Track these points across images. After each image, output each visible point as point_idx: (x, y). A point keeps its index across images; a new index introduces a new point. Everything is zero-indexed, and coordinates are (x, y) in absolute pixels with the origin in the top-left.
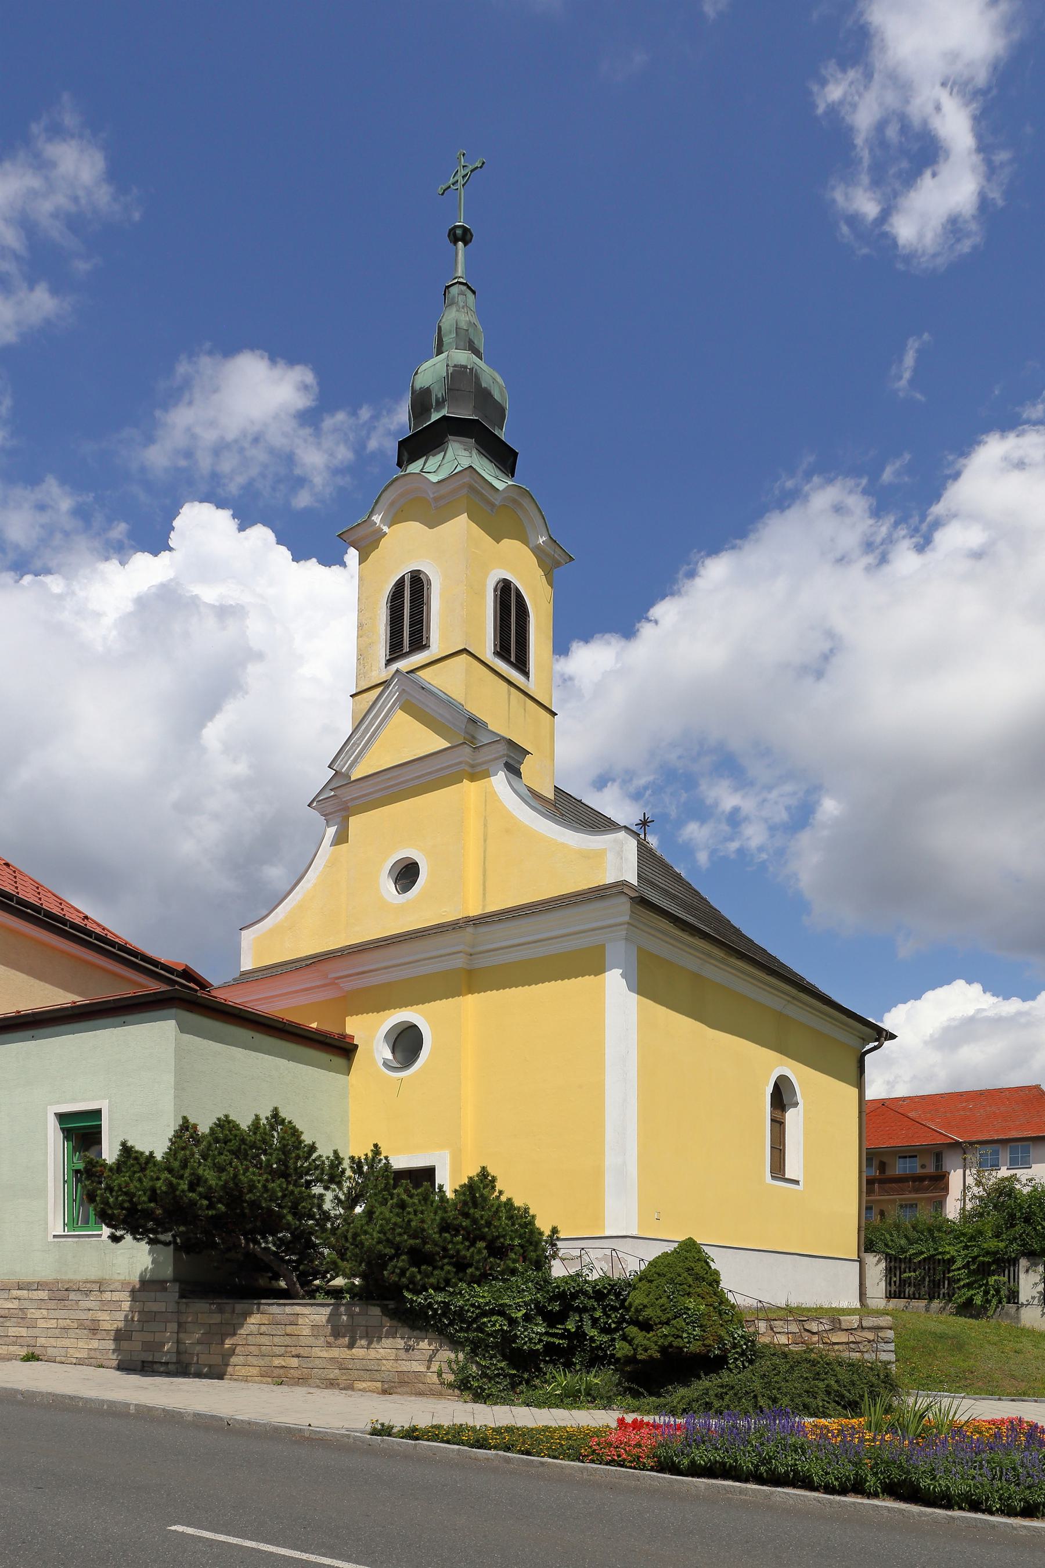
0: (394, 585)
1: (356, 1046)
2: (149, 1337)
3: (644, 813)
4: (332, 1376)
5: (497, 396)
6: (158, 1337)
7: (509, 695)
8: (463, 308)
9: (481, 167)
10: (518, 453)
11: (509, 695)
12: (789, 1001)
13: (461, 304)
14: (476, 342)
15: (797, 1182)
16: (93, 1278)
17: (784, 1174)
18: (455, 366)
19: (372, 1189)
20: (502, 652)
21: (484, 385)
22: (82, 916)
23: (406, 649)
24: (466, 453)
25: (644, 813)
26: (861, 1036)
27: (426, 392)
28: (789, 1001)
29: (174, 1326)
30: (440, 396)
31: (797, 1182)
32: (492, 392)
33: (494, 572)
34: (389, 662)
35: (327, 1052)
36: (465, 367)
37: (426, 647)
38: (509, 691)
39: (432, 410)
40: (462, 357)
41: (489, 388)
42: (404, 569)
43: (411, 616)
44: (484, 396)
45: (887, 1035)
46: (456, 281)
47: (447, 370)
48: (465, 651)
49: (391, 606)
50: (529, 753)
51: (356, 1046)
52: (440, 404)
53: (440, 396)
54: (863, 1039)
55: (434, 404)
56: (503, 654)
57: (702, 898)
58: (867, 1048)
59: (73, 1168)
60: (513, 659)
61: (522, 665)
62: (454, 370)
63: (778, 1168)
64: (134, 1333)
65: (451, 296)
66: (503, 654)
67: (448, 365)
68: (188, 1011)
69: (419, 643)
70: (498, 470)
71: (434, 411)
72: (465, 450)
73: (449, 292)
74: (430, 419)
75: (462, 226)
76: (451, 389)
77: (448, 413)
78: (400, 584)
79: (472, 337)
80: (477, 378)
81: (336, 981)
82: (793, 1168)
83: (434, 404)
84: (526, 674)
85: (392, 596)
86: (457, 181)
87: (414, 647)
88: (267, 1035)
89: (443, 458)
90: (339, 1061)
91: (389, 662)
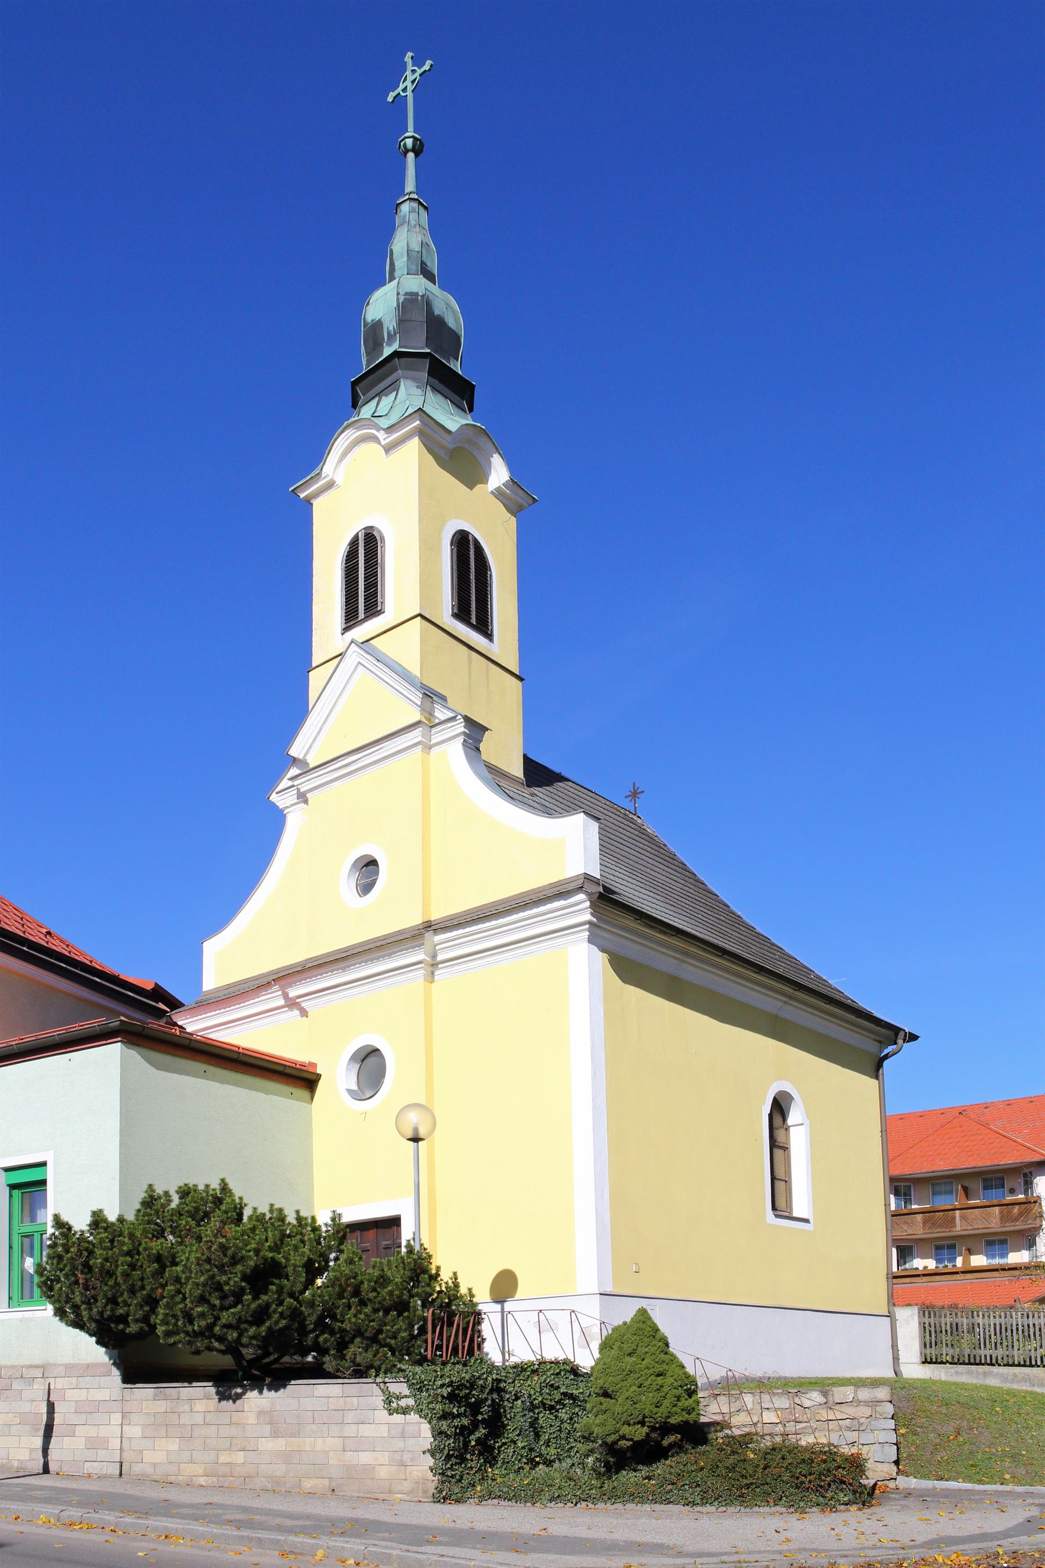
0: (349, 544)
1: (319, 1076)
2: (92, 1432)
3: (634, 783)
4: (279, 1474)
5: (451, 323)
6: (103, 1432)
7: (470, 662)
8: (415, 227)
9: (429, 70)
10: (474, 386)
11: (470, 662)
12: (785, 1002)
13: (413, 223)
14: (429, 264)
15: (806, 1221)
16: (37, 1362)
17: (791, 1212)
18: (406, 294)
19: (136, 1321)
20: (461, 613)
21: (437, 312)
22: (44, 931)
23: (361, 616)
24: (419, 392)
25: (634, 783)
26: (877, 1038)
27: (378, 325)
28: (785, 1002)
29: (117, 1418)
30: (391, 328)
31: (806, 1221)
32: (446, 321)
33: (449, 523)
34: (346, 630)
35: (287, 1084)
36: (417, 294)
37: (380, 612)
38: (469, 657)
39: (385, 344)
40: (417, 284)
41: (442, 315)
42: (355, 528)
43: (366, 578)
44: (436, 326)
45: (905, 1036)
46: (407, 197)
47: (398, 299)
48: (420, 615)
49: (346, 567)
50: (487, 729)
51: (319, 1076)
52: (391, 338)
53: (391, 328)
54: (880, 1042)
55: (386, 338)
56: (462, 615)
57: (698, 881)
58: (886, 1052)
59: (20, 1231)
60: (474, 621)
61: (483, 627)
62: (405, 299)
63: (780, 1206)
64: (11, 1449)
65: (402, 214)
66: (462, 615)
67: (398, 294)
68: (134, 1044)
69: (373, 608)
70: (454, 407)
71: (387, 345)
72: (417, 387)
73: (401, 211)
74: (382, 354)
75: (413, 137)
76: (402, 320)
77: (400, 346)
78: (354, 543)
79: (424, 259)
80: (429, 305)
81: (298, 1001)
82: (800, 1206)
83: (386, 338)
84: (489, 636)
85: (347, 556)
86: (406, 87)
87: (369, 614)
88: (221, 1067)
89: (395, 398)
90: (305, 1093)
91: (346, 630)
